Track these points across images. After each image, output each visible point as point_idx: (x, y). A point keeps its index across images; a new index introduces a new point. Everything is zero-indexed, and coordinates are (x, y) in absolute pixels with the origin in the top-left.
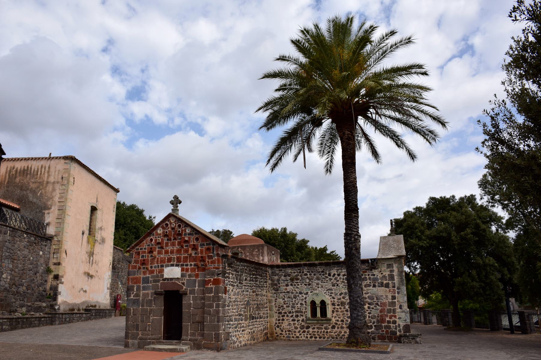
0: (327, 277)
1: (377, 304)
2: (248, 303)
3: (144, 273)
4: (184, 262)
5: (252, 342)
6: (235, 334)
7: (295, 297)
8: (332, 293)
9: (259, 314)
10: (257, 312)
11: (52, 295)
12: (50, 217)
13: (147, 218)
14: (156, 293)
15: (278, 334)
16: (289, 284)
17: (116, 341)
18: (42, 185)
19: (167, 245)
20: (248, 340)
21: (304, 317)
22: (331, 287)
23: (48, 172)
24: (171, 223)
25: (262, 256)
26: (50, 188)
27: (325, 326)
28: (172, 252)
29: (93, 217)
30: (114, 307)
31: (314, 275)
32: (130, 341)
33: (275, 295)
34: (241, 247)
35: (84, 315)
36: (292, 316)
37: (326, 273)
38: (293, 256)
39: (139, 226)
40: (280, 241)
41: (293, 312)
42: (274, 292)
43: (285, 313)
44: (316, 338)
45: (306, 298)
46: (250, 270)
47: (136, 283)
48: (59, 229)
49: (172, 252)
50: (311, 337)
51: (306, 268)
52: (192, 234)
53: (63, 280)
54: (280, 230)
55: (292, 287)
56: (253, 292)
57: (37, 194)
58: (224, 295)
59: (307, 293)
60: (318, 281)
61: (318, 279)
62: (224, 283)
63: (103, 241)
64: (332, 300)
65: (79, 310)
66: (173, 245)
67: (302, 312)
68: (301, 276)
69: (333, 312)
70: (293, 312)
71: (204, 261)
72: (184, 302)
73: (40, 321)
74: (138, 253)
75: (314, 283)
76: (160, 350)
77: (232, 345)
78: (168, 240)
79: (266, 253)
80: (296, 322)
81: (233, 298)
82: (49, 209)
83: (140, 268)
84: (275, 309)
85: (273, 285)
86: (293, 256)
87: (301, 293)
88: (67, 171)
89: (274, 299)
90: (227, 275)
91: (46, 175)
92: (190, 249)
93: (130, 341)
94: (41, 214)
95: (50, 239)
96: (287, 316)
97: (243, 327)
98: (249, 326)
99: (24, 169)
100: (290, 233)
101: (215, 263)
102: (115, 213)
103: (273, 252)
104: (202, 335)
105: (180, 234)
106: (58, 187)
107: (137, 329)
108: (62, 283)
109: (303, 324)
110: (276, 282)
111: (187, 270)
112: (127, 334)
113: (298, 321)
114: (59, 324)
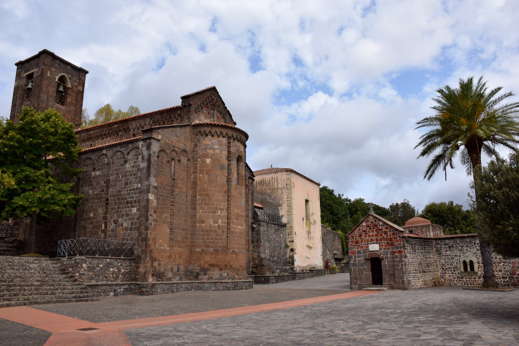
0: (473, 245)
1: (509, 263)
2: (420, 263)
3: (358, 248)
4: (380, 241)
5: (425, 286)
6: (413, 281)
7: (452, 258)
8: (477, 256)
9: (428, 269)
10: (427, 269)
11: (291, 261)
12: (283, 212)
13: (337, 196)
14: (366, 259)
15: (443, 282)
16: (448, 250)
17: (345, 287)
18: (275, 190)
19: (369, 232)
20: (422, 285)
21: (459, 271)
22: (476, 252)
23: (277, 181)
24: (370, 219)
25: (429, 232)
26: (279, 192)
27: (474, 277)
28: (373, 236)
29: (307, 206)
30: (326, 268)
31: (465, 244)
32: (353, 286)
33: (439, 257)
34: (414, 227)
35: (310, 274)
36: (451, 271)
37: (472, 243)
38: (460, 225)
39: (332, 204)
40: (448, 213)
41: (452, 268)
42: (438, 255)
43: (447, 269)
44: (468, 284)
45: (459, 259)
46: (420, 243)
47: (353, 254)
48: (290, 219)
49: (373, 236)
50: (465, 284)
51: (459, 239)
52: (383, 225)
53: (296, 252)
54: (447, 203)
55: (450, 252)
56: (423, 256)
57: (272, 197)
58: (405, 259)
59: (460, 256)
60: (467, 248)
61: (467, 246)
62: (404, 252)
63: (315, 222)
64: (478, 260)
65: (306, 271)
66: (373, 231)
67: (458, 268)
68: (455, 245)
69: (479, 268)
70: (452, 268)
71: (392, 240)
72: (382, 264)
73: (288, 278)
74: (353, 237)
75: (465, 249)
76: (371, 290)
77: (412, 287)
78: (369, 229)
79: (431, 230)
80: (454, 274)
81: (411, 260)
82: (281, 206)
83: (355, 246)
84: (439, 266)
85: (437, 251)
86: (460, 225)
87: (456, 256)
88: (289, 179)
89: (438, 260)
90: (406, 247)
91: (276, 183)
92: (383, 234)
93: (353, 286)
94: (276, 210)
95: (284, 226)
96: (448, 271)
97: (418, 277)
98: (422, 277)
99: (261, 181)
100: (457, 205)
101: (398, 241)
102: (319, 201)
103: (437, 228)
104: (395, 282)
105: (376, 226)
106: (284, 191)
107: (357, 279)
108: (296, 254)
109: (459, 275)
110: (439, 249)
111: (382, 246)
112: (351, 284)
113: (455, 274)
114: (299, 280)
